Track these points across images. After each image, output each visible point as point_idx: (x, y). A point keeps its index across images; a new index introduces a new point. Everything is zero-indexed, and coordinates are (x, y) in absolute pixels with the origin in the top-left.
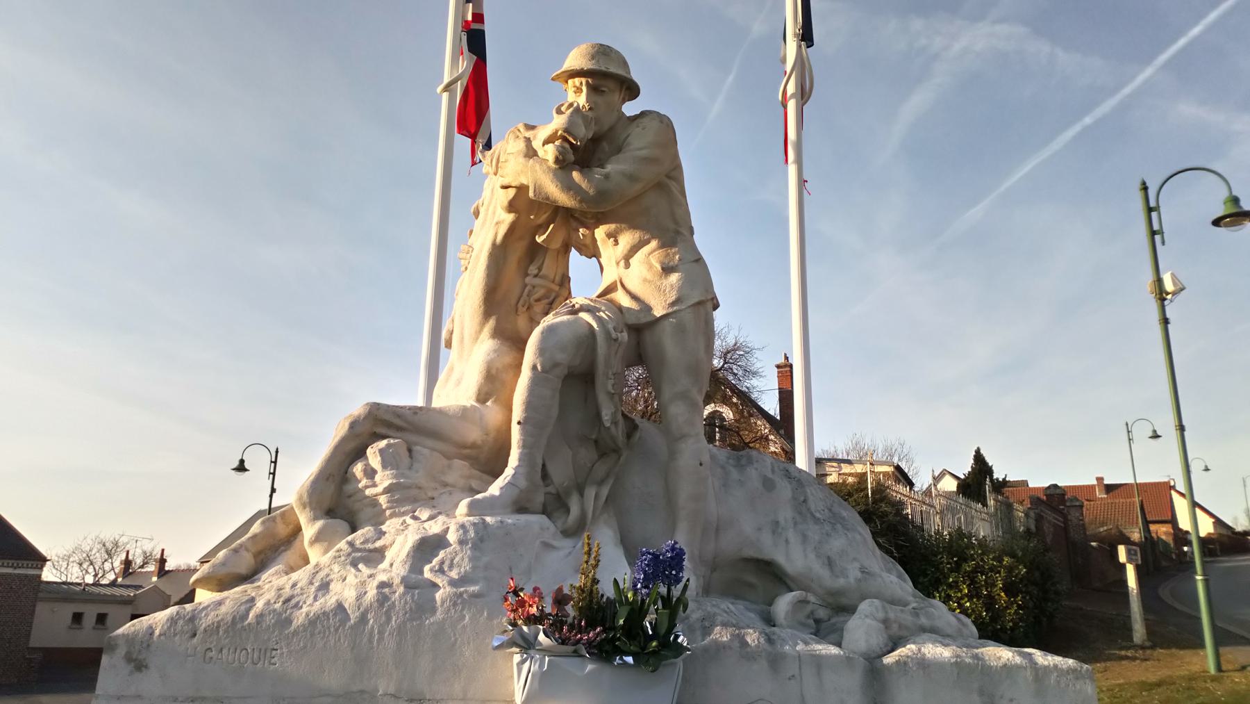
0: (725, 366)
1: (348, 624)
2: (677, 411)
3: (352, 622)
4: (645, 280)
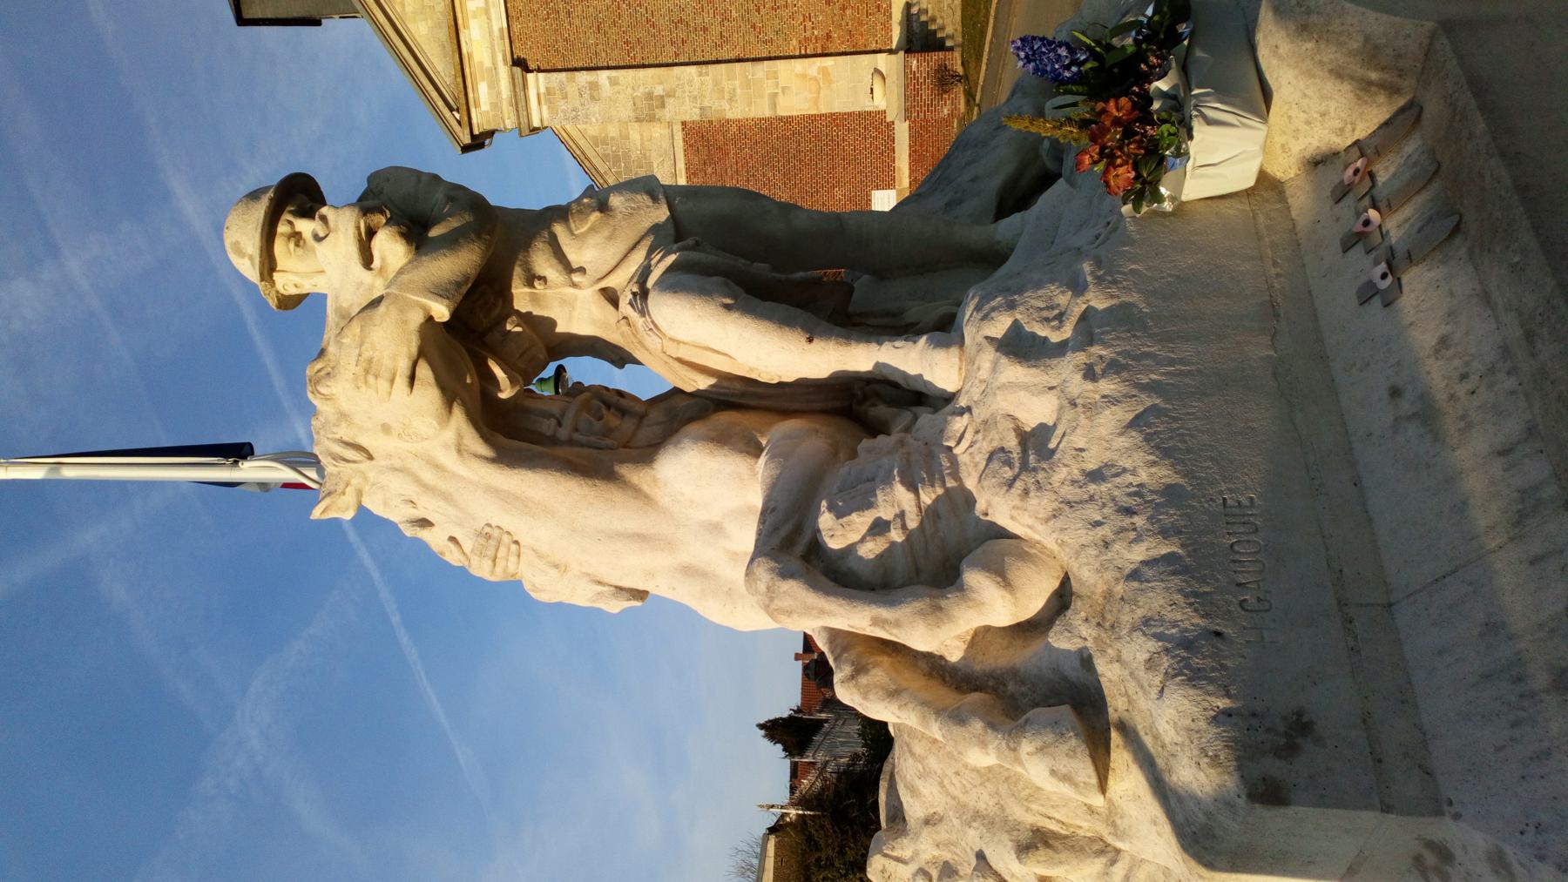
1: (1162, 405)
3: (1158, 401)
4: (610, 238)
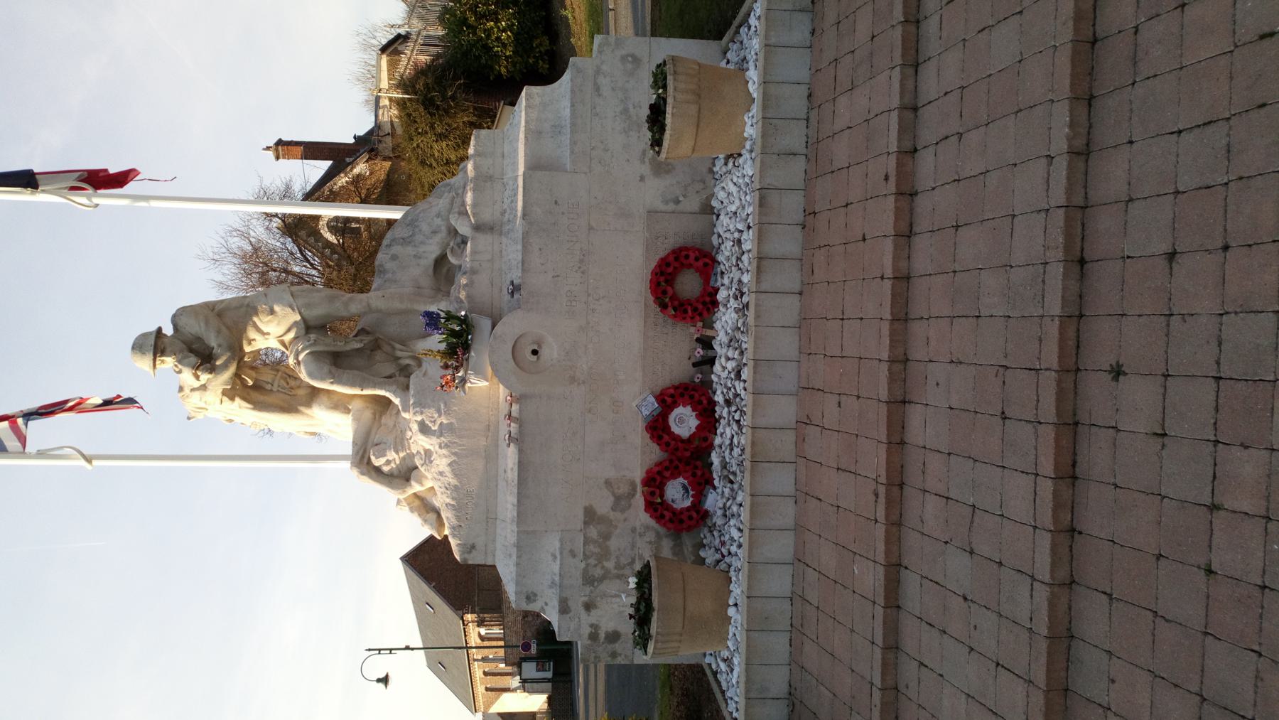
4: (278, 324)
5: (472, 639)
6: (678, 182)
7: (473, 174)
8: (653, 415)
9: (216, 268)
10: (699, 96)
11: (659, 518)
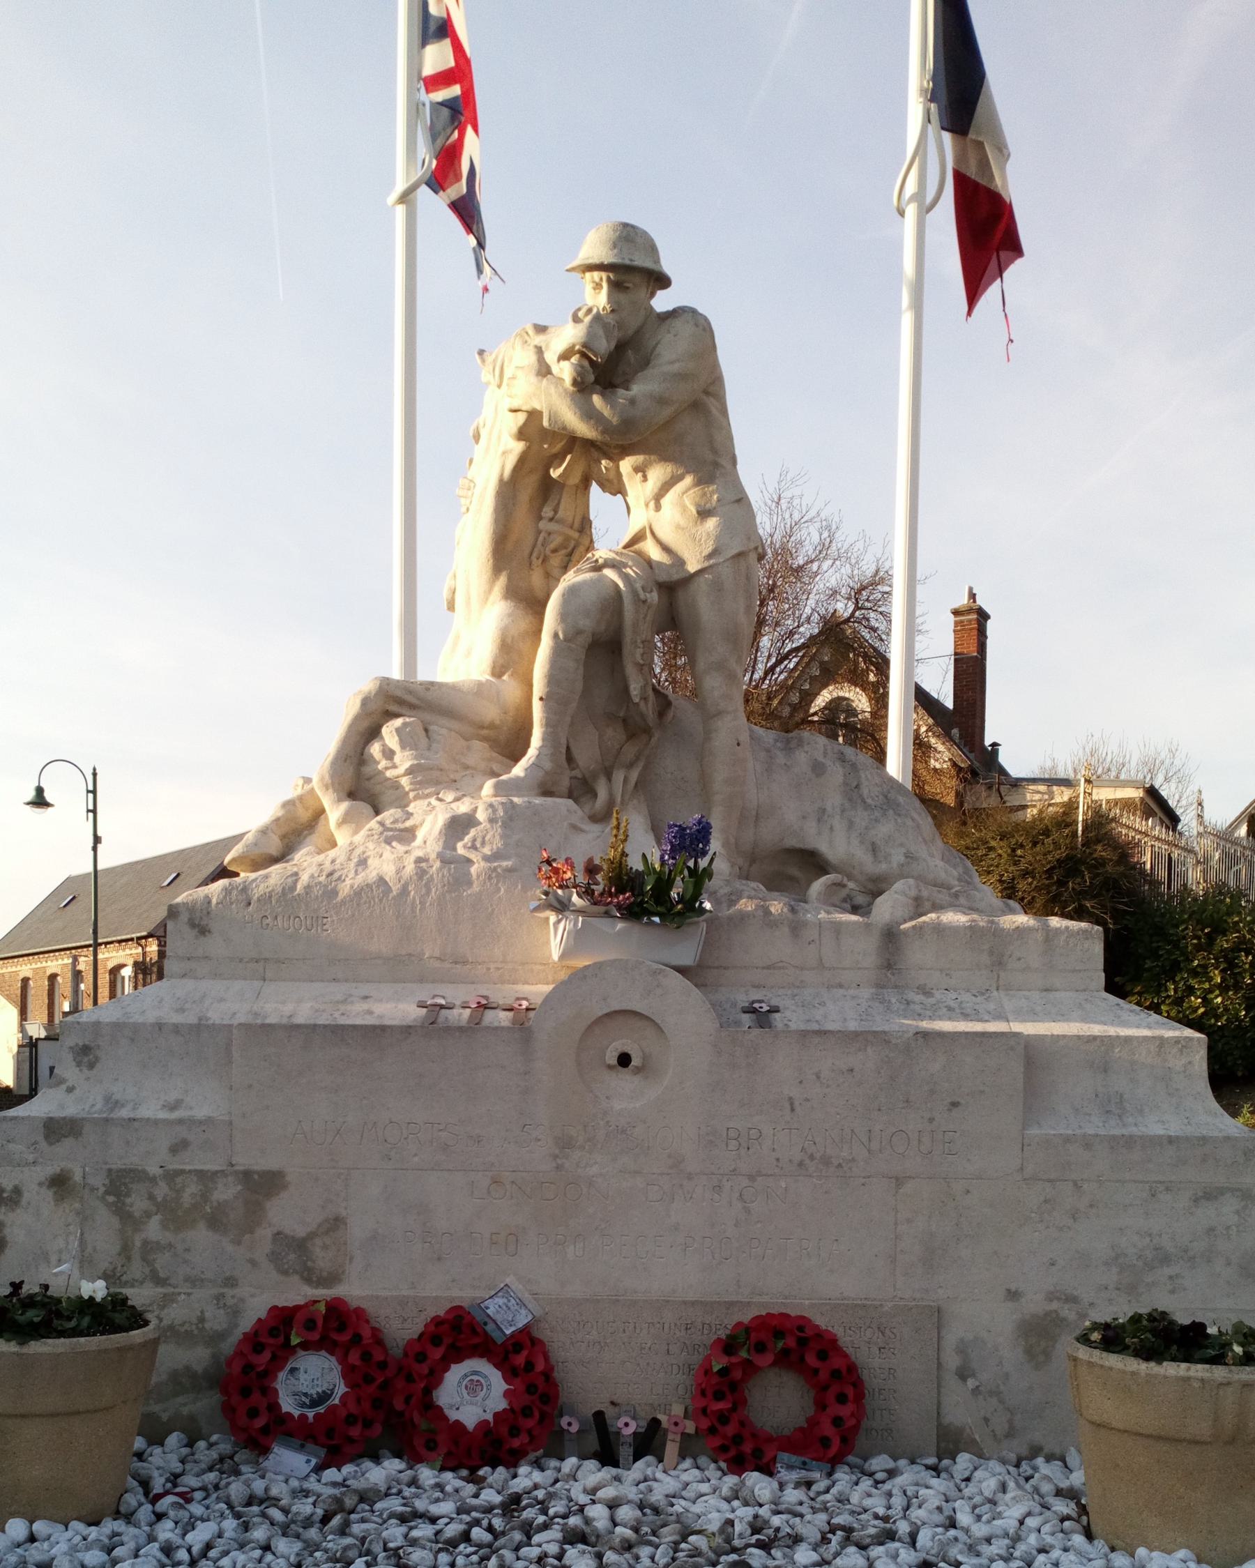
0: (857, 614)
2: (713, 684)
3: (395, 893)
4: (678, 527)
5: (114, 954)
6: (1007, 1376)
7: (1007, 926)
8: (485, 1324)
9: (766, 505)
10: (1232, 1441)
11: (254, 1340)
